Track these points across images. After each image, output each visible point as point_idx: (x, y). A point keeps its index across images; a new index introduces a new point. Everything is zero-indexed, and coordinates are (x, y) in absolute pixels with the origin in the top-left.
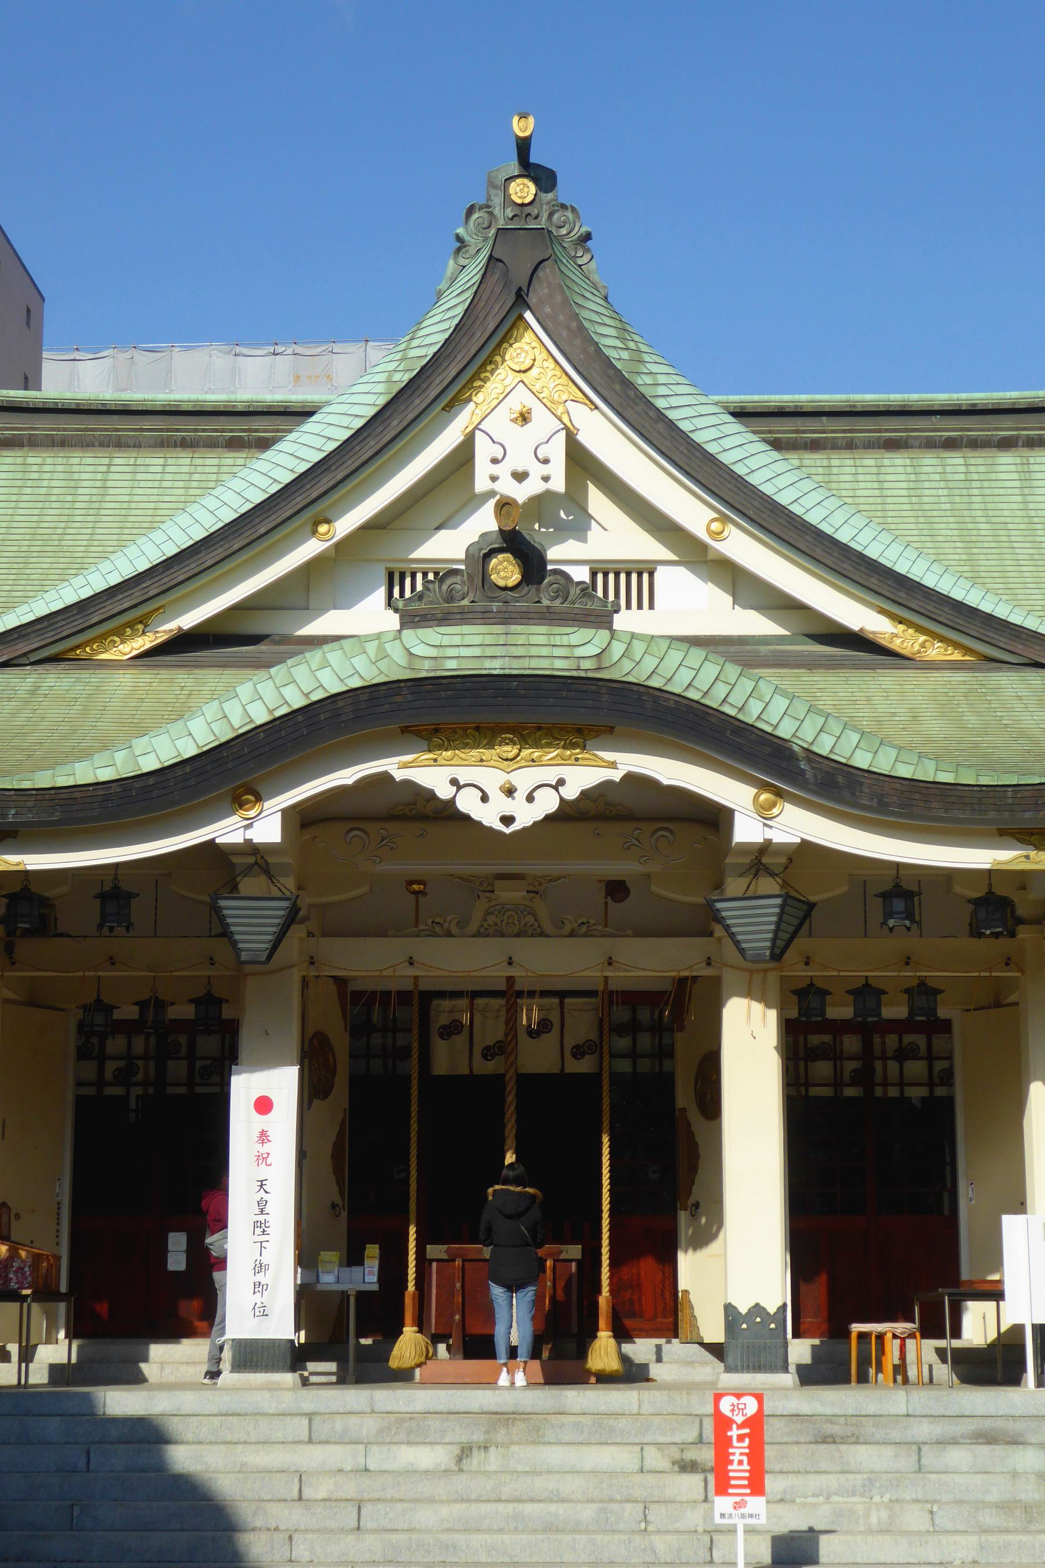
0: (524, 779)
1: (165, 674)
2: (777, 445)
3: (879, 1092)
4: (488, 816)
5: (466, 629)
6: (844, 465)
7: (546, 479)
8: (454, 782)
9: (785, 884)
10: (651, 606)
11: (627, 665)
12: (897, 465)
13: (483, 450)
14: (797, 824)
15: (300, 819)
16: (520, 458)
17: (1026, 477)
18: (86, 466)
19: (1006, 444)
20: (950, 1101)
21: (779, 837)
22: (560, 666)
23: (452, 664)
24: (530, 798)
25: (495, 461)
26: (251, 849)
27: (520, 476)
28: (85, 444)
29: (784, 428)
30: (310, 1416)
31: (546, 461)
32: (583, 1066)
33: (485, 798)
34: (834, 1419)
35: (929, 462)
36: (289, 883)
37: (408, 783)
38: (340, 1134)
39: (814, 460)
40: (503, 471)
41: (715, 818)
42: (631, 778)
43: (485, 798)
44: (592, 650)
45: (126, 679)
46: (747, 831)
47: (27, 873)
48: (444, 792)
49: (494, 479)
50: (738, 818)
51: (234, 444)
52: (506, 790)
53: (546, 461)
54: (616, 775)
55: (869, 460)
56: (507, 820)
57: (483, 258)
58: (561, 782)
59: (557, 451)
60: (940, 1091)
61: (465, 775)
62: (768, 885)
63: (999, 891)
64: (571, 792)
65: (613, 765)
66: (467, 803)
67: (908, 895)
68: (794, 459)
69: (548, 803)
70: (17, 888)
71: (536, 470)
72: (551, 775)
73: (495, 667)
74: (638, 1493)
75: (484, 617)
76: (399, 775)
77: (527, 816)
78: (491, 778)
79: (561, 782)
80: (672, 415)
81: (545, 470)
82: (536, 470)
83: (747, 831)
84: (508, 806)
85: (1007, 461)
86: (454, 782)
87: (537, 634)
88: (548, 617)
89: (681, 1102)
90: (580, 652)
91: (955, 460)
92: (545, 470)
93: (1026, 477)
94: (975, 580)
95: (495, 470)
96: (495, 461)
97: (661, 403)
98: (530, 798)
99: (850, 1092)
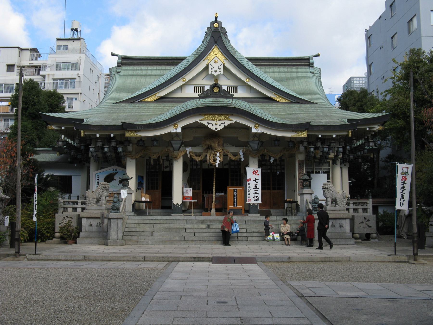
0: (219, 122)
1: (159, 104)
2: (256, 65)
3: (273, 171)
4: (213, 128)
5: (210, 99)
6: (268, 68)
7: (220, 72)
8: (208, 123)
9: (259, 139)
10: (237, 92)
11: (235, 105)
12: (276, 69)
13: (210, 67)
14: (260, 130)
15: (183, 128)
16: (216, 68)
17: (297, 71)
18: (144, 68)
19: (294, 65)
20: (284, 173)
21: (258, 132)
22: (225, 105)
23: (208, 105)
24: (220, 125)
25: (212, 69)
26: (176, 133)
27: (216, 71)
28: (144, 65)
29: (258, 62)
30: (186, 220)
31: (220, 69)
32: (227, 167)
33: (213, 125)
34: (193, 259)
35: (282, 68)
36: (181, 137)
37: (201, 123)
38: (189, 177)
39: (263, 68)
40: (213, 70)
41: (249, 129)
42: (235, 122)
43: (213, 125)
44: (230, 102)
45: (153, 105)
46: (254, 131)
47: (142, 137)
48: (206, 124)
49: (212, 72)
50: (252, 129)
51: (168, 65)
52: (216, 124)
53: (220, 69)
54: (233, 122)
55: (272, 68)
56: (216, 129)
57: (210, 36)
58: (225, 123)
59: (222, 67)
60: (283, 171)
61: (210, 122)
62: (256, 139)
63: (292, 140)
64: (226, 125)
65: (233, 120)
66: (210, 126)
67: (278, 141)
68: (260, 67)
69: (223, 126)
70: (139, 139)
71: (218, 70)
72: (223, 122)
73: (214, 105)
74: (247, 225)
75: (213, 97)
76: (199, 122)
77: (219, 128)
78: (214, 122)
79: (225, 123)
80: (240, 62)
81: (220, 70)
82: (218, 70)
83: (254, 131)
84: (216, 127)
85: (294, 68)
86: (208, 123)
87: (221, 100)
88: (222, 97)
89: (242, 173)
90: (228, 103)
91: (286, 68)
92: (220, 70)
93: (297, 71)
94: (289, 88)
95: (212, 70)
96: (212, 69)
97: (239, 60)
98: (220, 125)
99: (269, 171)
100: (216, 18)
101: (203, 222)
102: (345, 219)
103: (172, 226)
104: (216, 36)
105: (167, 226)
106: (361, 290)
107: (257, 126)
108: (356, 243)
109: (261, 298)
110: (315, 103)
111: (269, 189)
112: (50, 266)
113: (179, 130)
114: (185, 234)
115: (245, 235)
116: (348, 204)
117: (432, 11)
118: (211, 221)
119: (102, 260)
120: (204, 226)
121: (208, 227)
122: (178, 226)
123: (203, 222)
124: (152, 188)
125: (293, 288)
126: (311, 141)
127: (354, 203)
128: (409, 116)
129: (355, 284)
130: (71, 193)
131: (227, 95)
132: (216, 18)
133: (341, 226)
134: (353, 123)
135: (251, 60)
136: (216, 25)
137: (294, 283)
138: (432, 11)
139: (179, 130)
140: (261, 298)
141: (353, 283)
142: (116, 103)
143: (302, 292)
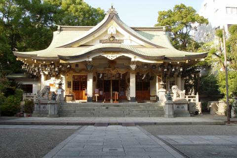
0: (113, 55)
4: (110, 59)
15: (93, 59)
32: (118, 79)
46: (133, 60)
48: (106, 56)
59: (115, 31)
66: (108, 57)
69: (115, 58)
77: (113, 58)
100: (112, 7)
101: (104, 106)
102: (185, 104)
103: (87, 108)
104: (219, 27)
105: (83, 108)
106: (207, 140)
107: (88, 57)
108: (191, 116)
109: (140, 146)
110: (163, 48)
111: (138, 90)
112: (8, 127)
113: (91, 60)
114: (93, 112)
115: (128, 112)
116: (185, 97)
117: (214, 1)
118: (108, 105)
119: (42, 125)
120: (104, 108)
121: (107, 108)
122: (90, 108)
123: (104, 106)
124: (76, 90)
125: (161, 139)
126: (162, 66)
127: (189, 97)
128: (24, 51)
129: (202, 137)
130: (32, 92)
131: (120, 42)
132: (112, 7)
133: (183, 107)
134: (187, 57)
135: (133, 28)
136: (112, 10)
137: (160, 136)
138: (214, 1)
139: (91, 60)
140: (140, 146)
141: (200, 136)
142: (163, 48)
143: (169, 142)
